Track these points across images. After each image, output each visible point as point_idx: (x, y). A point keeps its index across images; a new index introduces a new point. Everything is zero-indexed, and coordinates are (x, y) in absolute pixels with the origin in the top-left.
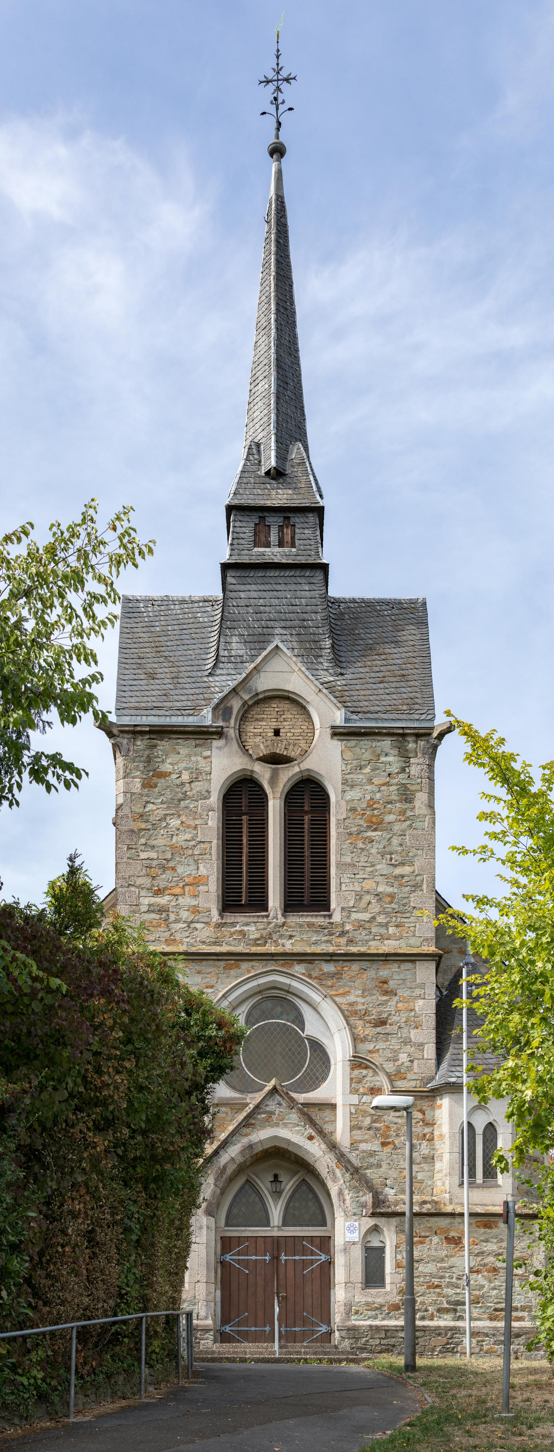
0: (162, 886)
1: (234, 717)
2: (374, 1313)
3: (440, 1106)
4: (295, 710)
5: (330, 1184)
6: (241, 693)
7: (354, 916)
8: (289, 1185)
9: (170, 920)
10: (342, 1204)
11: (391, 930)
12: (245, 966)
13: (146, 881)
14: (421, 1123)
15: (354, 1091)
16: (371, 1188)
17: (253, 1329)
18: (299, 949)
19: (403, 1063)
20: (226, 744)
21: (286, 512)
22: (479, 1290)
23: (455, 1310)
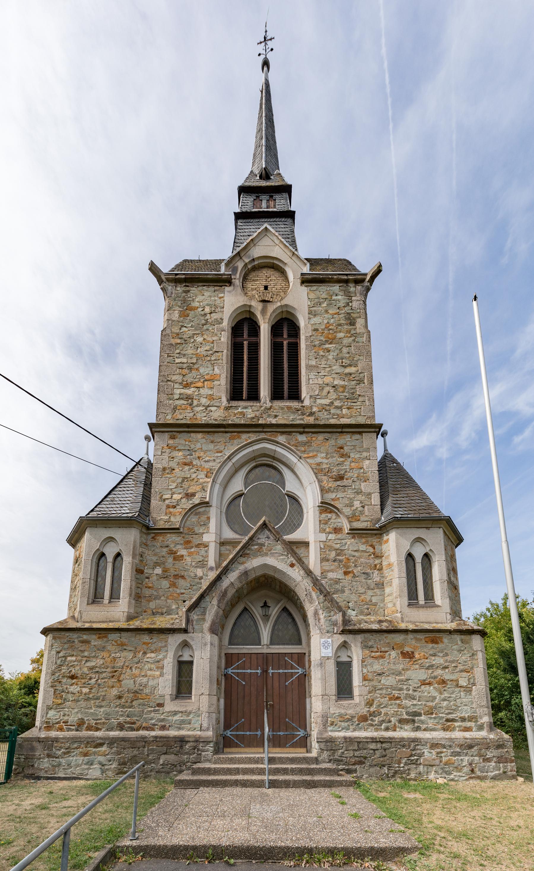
0: (189, 381)
1: (239, 273)
2: (346, 724)
3: (387, 541)
4: (277, 274)
6: (243, 258)
7: (319, 401)
8: (274, 611)
9: (194, 405)
10: (318, 623)
11: (345, 411)
13: (178, 378)
14: (372, 556)
15: (322, 531)
16: (340, 609)
17: (248, 733)
19: (357, 508)
20: (234, 289)
22: (432, 701)
23: (414, 721)
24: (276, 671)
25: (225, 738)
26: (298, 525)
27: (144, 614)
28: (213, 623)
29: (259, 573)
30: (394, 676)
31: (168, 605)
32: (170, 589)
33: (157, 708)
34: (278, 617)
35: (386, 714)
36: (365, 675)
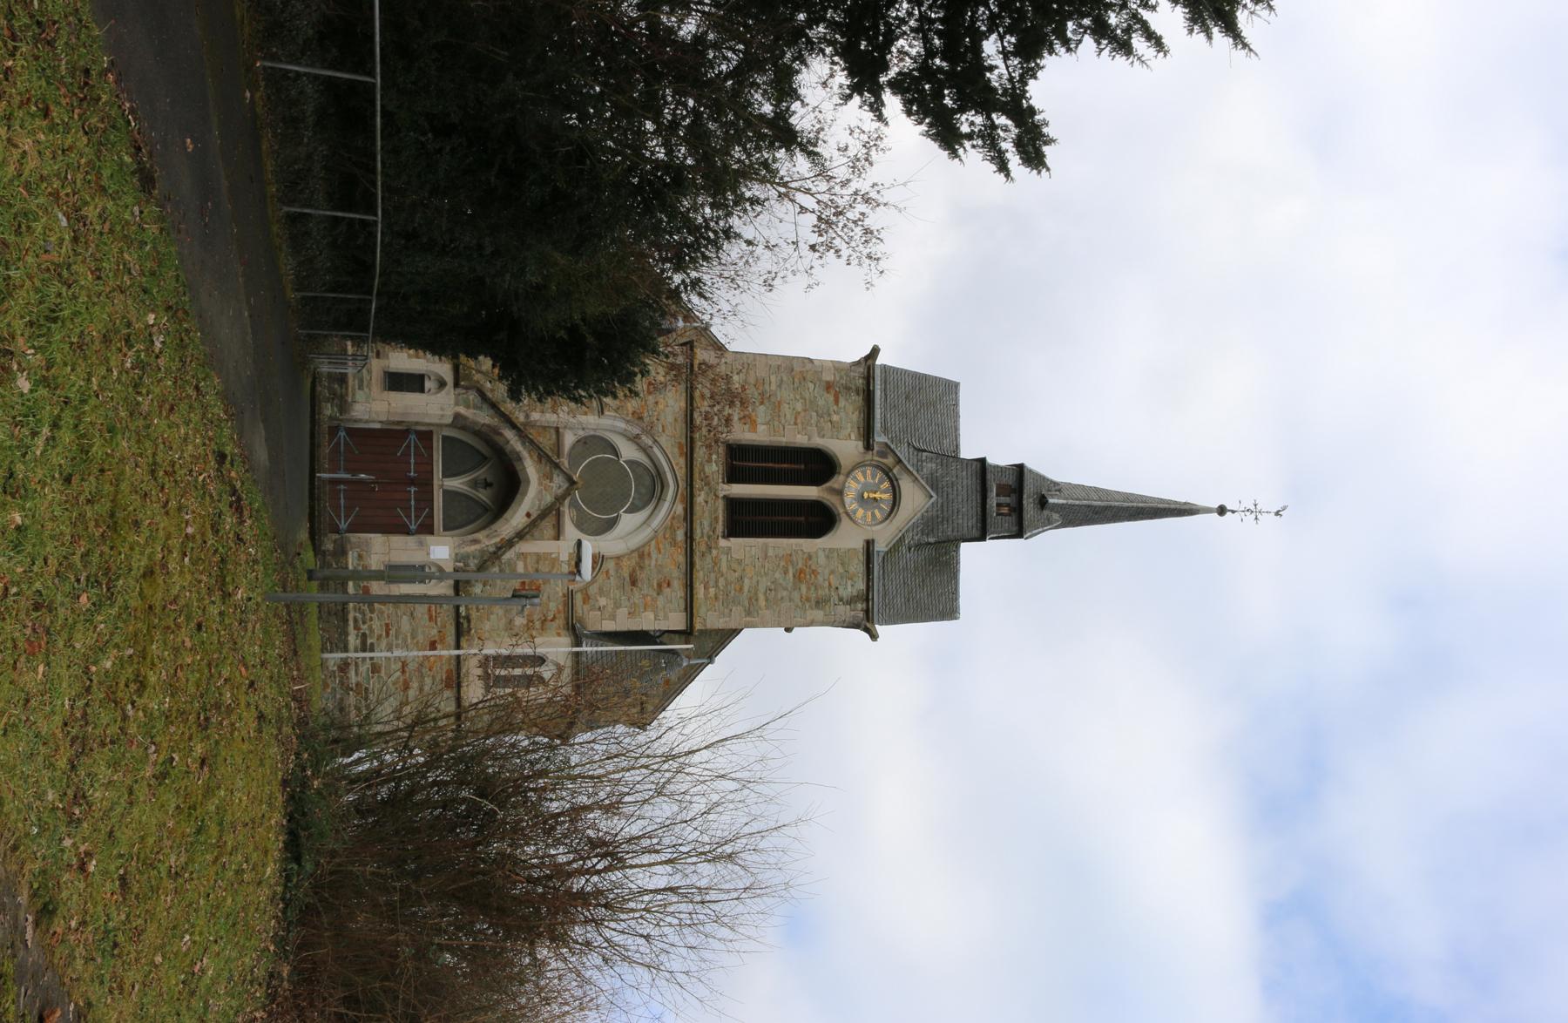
8: (483, 495)
12: (682, 461)
18: (697, 509)
21: (1018, 510)
28: (466, 418)
29: (521, 475)
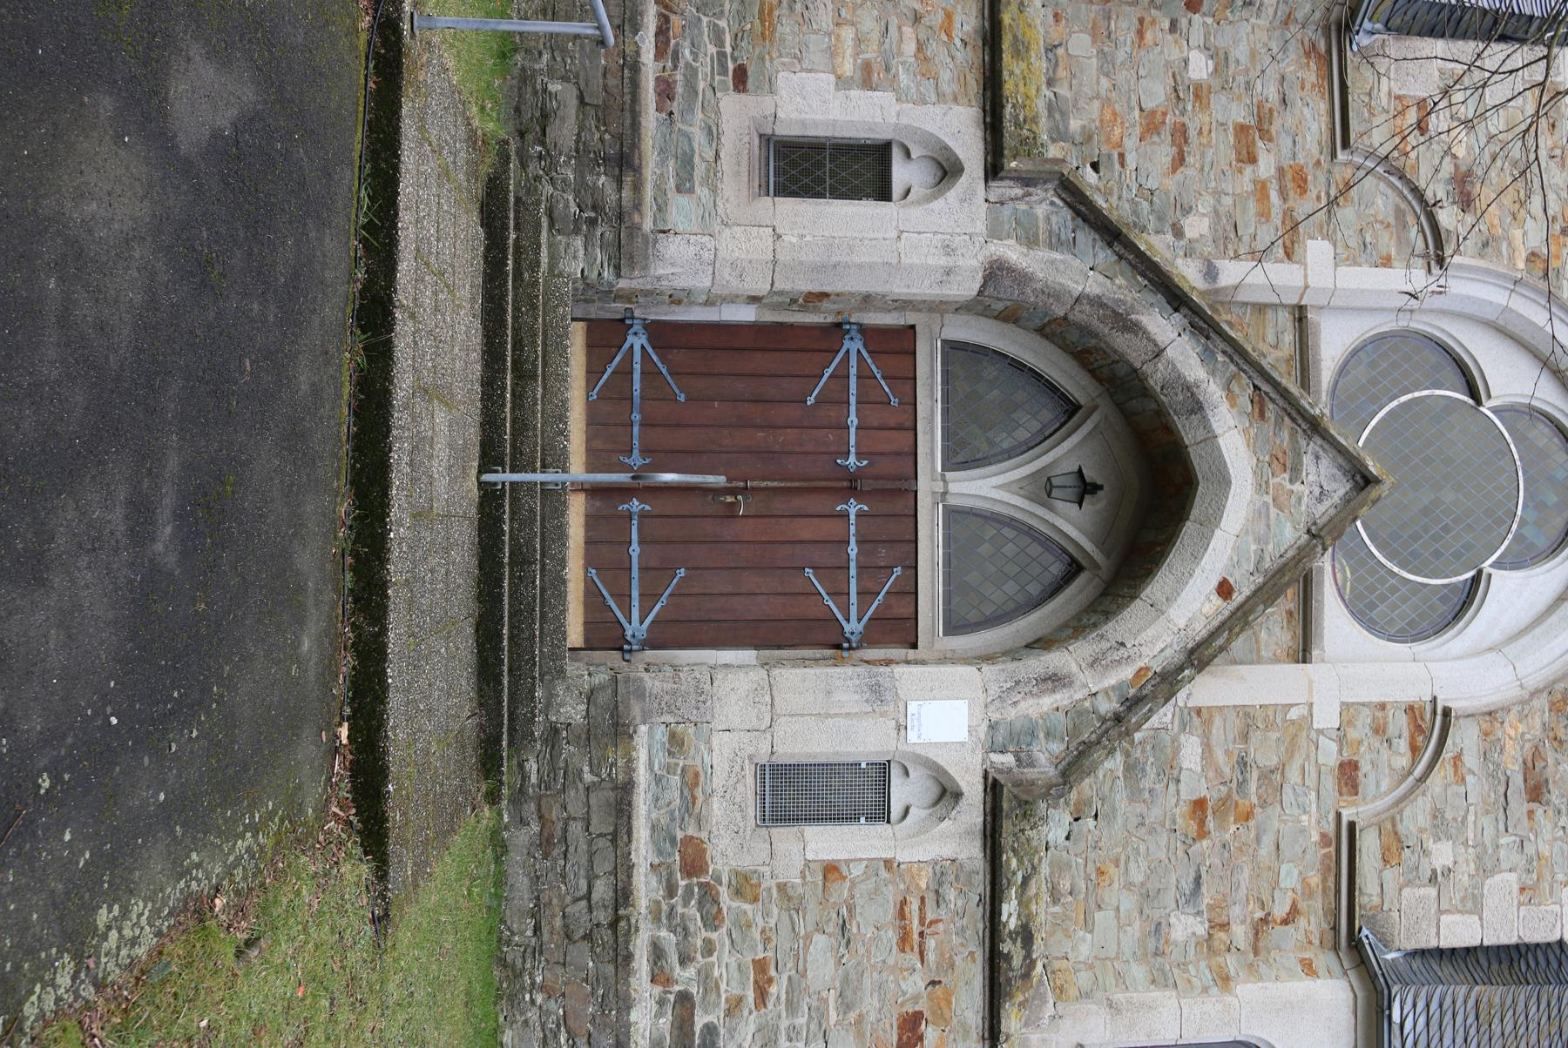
5: (1083, 649)
8: (1072, 524)
14: (1259, 914)
24: (853, 528)
25: (621, 325)
26: (1372, 621)
27: (1050, 12)
28: (1022, 278)
29: (1196, 456)
30: (838, 985)
31: (1081, 104)
32: (1137, 112)
33: (731, 66)
34: (1045, 541)
35: (709, 948)
36: (844, 869)
